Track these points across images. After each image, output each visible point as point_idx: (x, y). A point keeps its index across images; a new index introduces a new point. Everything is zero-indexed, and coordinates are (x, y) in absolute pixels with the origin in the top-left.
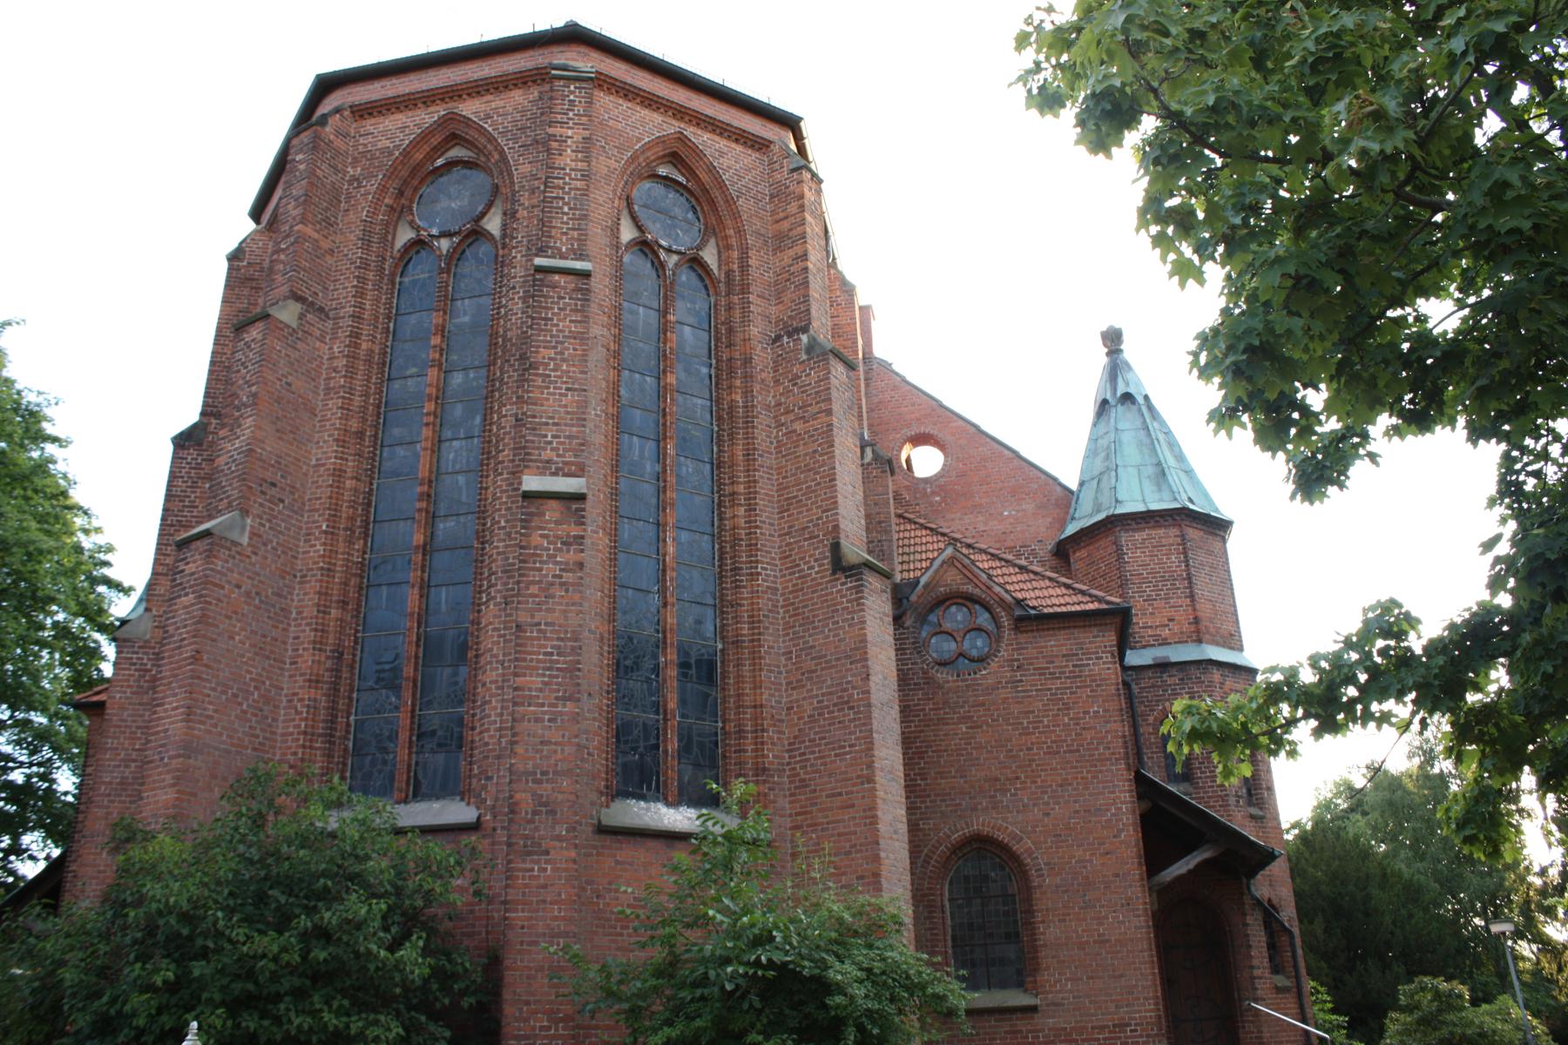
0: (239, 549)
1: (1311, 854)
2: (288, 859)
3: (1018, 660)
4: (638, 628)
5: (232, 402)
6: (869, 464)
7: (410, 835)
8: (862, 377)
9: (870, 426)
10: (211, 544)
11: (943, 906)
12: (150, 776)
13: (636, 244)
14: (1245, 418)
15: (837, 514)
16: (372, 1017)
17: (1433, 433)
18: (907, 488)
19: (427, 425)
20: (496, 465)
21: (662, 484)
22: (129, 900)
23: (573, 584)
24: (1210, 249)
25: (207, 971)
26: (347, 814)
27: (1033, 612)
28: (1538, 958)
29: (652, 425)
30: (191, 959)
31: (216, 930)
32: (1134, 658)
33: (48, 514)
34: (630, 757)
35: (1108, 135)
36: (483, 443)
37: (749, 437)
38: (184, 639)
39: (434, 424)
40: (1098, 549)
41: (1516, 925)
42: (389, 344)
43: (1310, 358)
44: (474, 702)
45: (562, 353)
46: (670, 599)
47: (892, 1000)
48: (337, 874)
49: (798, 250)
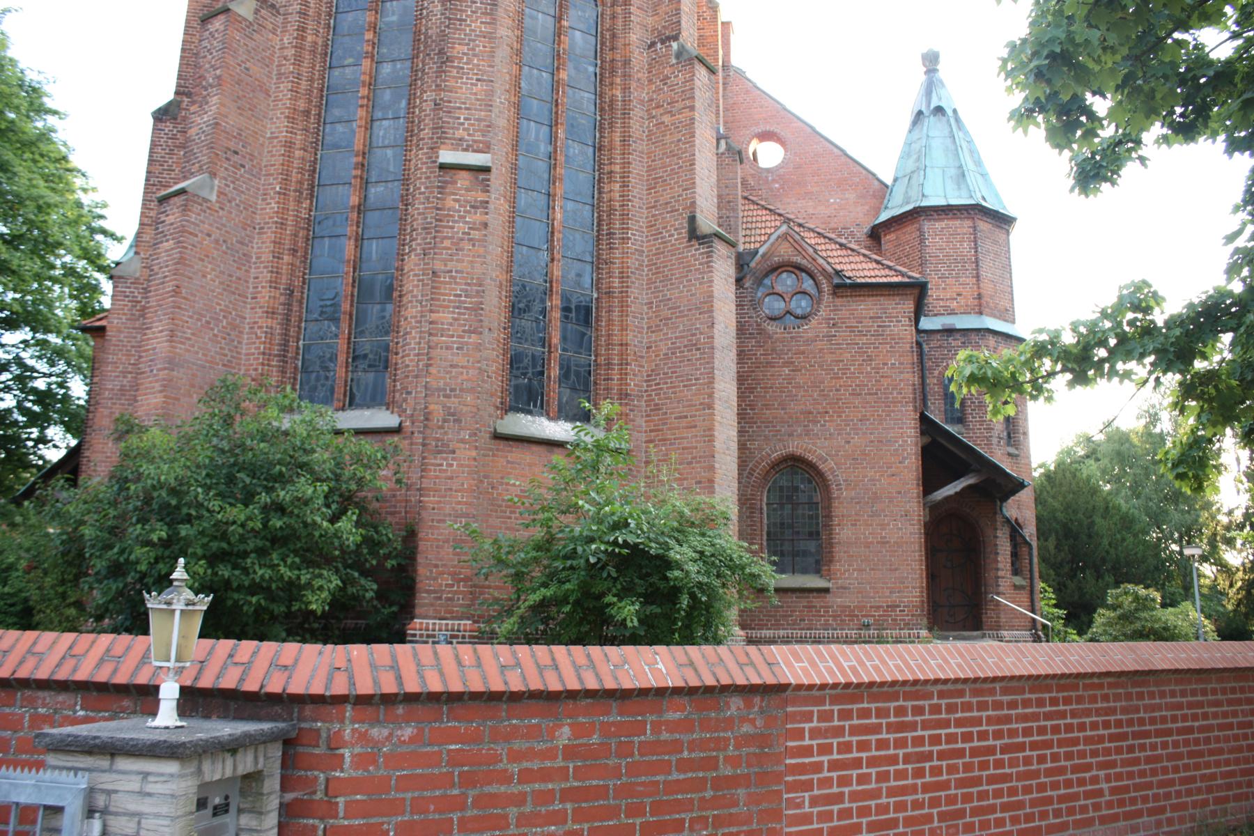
1: (1052, 488)
2: (251, 450)
3: (834, 319)
4: (531, 278)
5: (201, 82)
6: (723, 154)
7: (346, 434)
8: (721, 81)
9: (725, 123)
10: (187, 200)
11: (761, 509)
12: (142, 384)
14: (1040, 118)
15: (695, 192)
16: (317, 571)
17: (1197, 143)
18: (753, 176)
19: (362, 106)
20: (418, 141)
21: (553, 162)
22: (130, 476)
23: (479, 240)
25: (191, 532)
26: (297, 417)
27: (848, 281)
28: (1216, 577)
29: (547, 113)
30: (179, 523)
31: (197, 501)
32: (926, 323)
33: (53, 175)
34: (520, 381)
36: (408, 123)
37: (625, 126)
38: (166, 277)
39: (367, 106)
40: (904, 234)
41: (1204, 551)
42: (330, 37)
44: (398, 332)
45: (473, 49)
46: (557, 256)
47: (718, 576)
48: (289, 463)
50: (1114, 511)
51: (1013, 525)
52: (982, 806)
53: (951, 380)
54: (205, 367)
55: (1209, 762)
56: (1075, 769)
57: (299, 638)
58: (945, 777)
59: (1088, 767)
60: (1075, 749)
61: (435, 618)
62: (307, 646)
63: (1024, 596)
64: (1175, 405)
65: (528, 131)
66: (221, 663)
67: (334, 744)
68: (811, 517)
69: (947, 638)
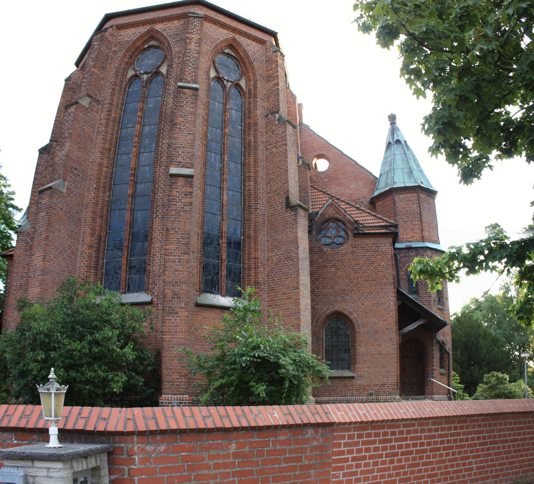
0: (62, 194)
2: (82, 314)
5: (62, 136)
6: (301, 166)
8: (298, 131)
9: (301, 151)
10: (52, 192)
11: (322, 338)
12: (30, 282)
13: (216, 78)
14: (442, 150)
16: (116, 373)
17: (513, 158)
18: (315, 175)
19: (135, 146)
22: (26, 328)
23: (188, 211)
24: (428, 85)
25: (56, 355)
26: (103, 298)
30: (50, 351)
34: (208, 277)
35: (388, 41)
37: (256, 154)
41: (530, 355)
43: (467, 127)
44: (150, 254)
45: (186, 120)
46: (225, 218)
47: (303, 372)
49: (275, 81)
50: (489, 336)
51: (441, 344)
52: (419, 476)
53: (411, 272)
54: (59, 274)
55: (523, 454)
56: (462, 459)
57: (110, 405)
58: (403, 463)
59: (467, 458)
60: (463, 450)
61: (172, 394)
62: (114, 409)
63: (445, 379)
64: (517, 283)
65: (211, 157)
66: (75, 417)
67: (130, 453)
68: (346, 342)
69: (408, 399)
